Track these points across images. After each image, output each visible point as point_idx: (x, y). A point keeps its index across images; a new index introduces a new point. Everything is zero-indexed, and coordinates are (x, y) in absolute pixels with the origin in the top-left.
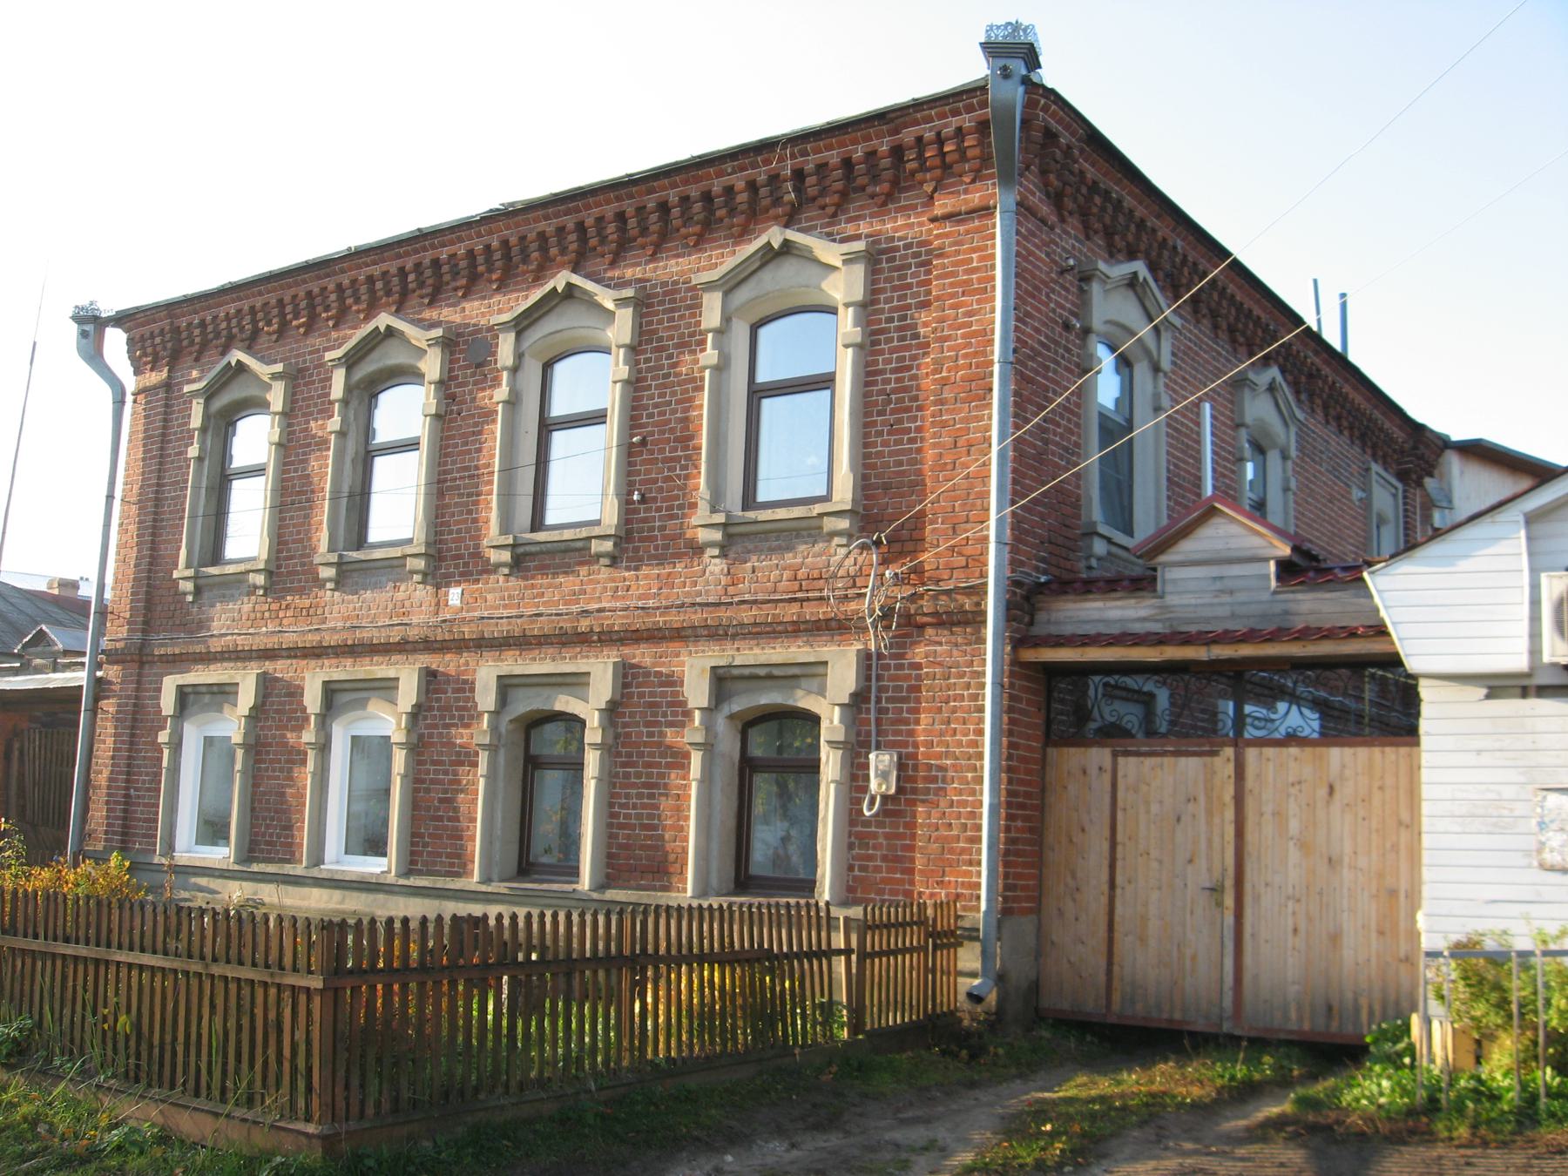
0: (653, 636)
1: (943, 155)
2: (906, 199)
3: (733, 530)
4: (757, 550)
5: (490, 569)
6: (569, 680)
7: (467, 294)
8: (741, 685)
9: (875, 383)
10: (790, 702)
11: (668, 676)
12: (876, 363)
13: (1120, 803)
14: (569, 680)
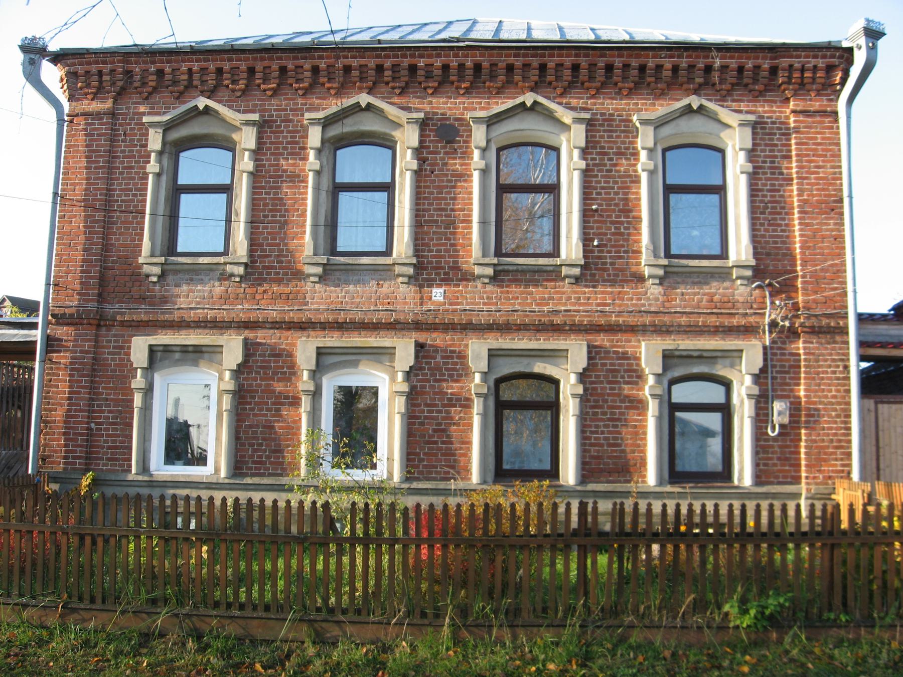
0: (611, 329)
1: (802, 77)
2: (770, 96)
3: (166, 267)
4: (684, 282)
5: (468, 277)
6: (546, 353)
7: (436, 92)
8: (676, 361)
9: (757, 196)
10: (714, 372)
11: (623, 353)
12: (757, 184)
13: (880, 427)
14: (546, 353)
